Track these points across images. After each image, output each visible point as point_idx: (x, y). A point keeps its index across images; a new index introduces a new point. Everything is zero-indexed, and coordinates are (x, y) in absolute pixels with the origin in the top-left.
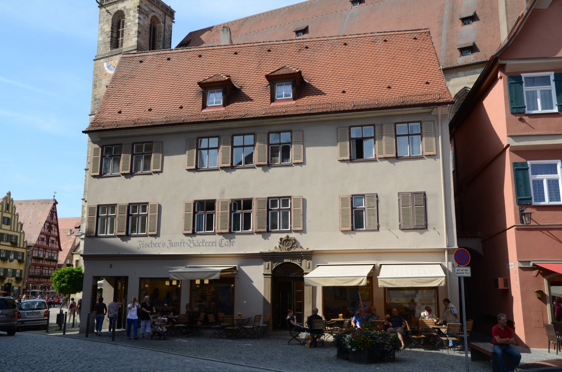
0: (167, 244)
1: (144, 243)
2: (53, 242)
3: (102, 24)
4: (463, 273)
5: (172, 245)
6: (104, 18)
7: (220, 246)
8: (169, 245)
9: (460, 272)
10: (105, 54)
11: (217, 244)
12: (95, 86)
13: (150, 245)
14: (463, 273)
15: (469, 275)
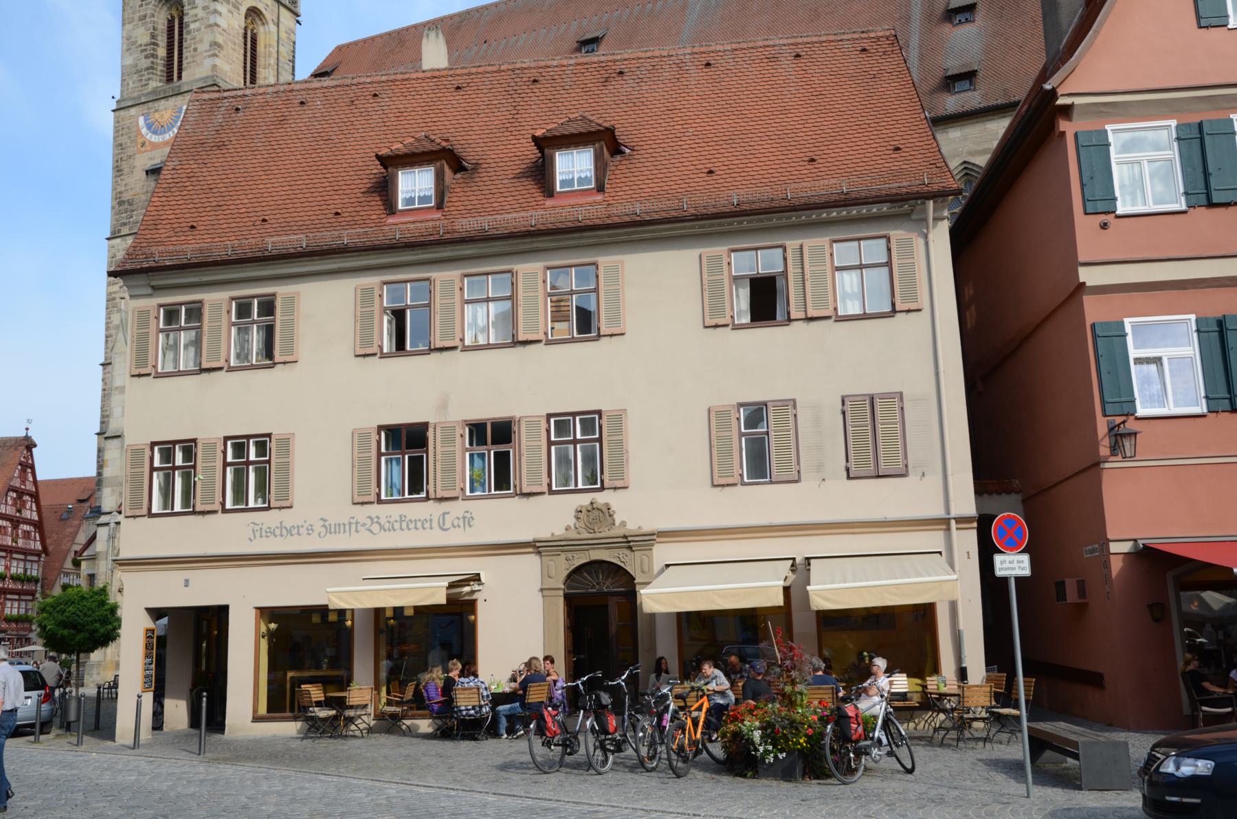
0: (318, 527)
1: (264, 528)
2: (27, 535)
3: (129, 27)
4: (1013, 569)
5: (329, 529)
6: (134, 13)
7: (441, 528)
8: (323, 530)
9: (1007, 565)
10: (139, 97)
11: (435, 524)
12: (118, 170)
13: (278, 532)
14: (1013, 569)
15: (1027, 572)
